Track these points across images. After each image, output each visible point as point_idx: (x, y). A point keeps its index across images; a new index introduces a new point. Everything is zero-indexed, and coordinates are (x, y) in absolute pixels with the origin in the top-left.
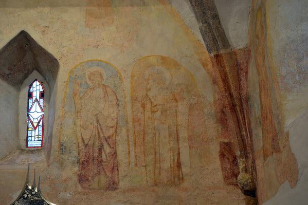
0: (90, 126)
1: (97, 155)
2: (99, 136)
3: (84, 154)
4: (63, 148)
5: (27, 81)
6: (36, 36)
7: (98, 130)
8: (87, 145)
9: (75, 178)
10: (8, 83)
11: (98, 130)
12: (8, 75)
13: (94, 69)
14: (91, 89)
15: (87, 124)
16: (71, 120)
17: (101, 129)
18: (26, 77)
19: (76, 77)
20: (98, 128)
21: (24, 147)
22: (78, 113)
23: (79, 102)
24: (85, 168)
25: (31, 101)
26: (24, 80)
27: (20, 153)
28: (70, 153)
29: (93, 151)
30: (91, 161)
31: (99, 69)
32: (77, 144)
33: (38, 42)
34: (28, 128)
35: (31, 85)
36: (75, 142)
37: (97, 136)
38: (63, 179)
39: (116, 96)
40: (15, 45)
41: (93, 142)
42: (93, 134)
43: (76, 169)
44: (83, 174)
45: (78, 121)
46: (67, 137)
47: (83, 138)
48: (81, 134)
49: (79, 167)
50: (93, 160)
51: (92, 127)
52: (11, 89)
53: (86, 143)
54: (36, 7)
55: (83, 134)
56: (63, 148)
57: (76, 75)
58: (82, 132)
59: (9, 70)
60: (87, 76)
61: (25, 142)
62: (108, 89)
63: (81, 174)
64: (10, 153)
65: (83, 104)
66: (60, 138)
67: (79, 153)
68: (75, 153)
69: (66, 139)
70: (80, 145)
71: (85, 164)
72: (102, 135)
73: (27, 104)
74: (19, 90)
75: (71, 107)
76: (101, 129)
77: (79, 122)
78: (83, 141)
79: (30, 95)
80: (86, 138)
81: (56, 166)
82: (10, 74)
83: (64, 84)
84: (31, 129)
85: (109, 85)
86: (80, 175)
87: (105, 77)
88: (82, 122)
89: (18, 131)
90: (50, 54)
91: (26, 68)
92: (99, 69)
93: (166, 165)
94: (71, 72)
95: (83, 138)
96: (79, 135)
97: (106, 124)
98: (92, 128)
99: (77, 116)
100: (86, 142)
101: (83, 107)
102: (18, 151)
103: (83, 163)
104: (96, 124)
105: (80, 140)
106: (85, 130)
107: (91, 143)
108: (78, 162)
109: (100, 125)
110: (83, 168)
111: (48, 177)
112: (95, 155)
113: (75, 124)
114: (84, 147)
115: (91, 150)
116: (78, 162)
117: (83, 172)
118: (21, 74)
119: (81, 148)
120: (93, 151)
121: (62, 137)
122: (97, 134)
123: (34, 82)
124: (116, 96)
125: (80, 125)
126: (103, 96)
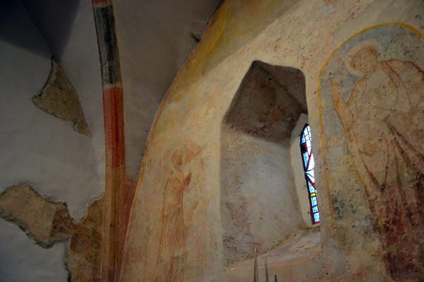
0: (379, 145)
1: (415, 201)
2: (407, 161)
3: (383, 207)
4: (337, 205)
5: (296, 131)
6: (268, 58)
7: (399, 147)
8: (384, 185)
9: (380, 267)
10: (267, 140)
11: (399, 147)
12: (262, 129)
13: (357, 48)
14: (362, 80)
15: (372, 142)
16: (340, 149)
17: (406, 142)
18: (292, 126)
19: (331, 76)
20: (397, 143)
21: (309, 224)
22: (348, 130)
23: (347, 111)
24: (395, 239)
25: (306, 155)
26: (291, 131)
27: (304, 235)
28: (354, 212)
29: (403, 196)
30: (404, 219)
31: (366, 43)
32: (363, 189)
33: (271, 64)
34: (310, 194)
35: (302, 133)
36: (357, 186)
37: (401, 160)
38: (354, 271)
39: (418, 68)
40: (253, 84)
41: (394, 176)
42: (392, 158)
43: (376, 243)
44: (395, 253)
45: (354, 144)
46: (340, 181)
47: (371, 175)
48: (365, 166)
49: (381, 239)
50: (409, 215)
51: (383, 145)
52: (275, 147)
53: (381, 182)
54: (264, 29)
55: (367, 165)
56: (337, 205)
57: (330, 73)
58: (366, 161)
59: (261, 121)
60: (348, 66)
61: (310, 215)
62: (394, 65)
63: (389, 255)
64: (287, 237)
65: (354, 113)
66: (328, 189)
67: (372, 208)
68: (364, 210)
69: (339, 187)
70: (370, 189)
71: (392, 230)
72: (411, 155)
73: (301, 160)
74: (288, 146)
75: (336, 126)
76: (406, 142)
77: (355, 148)
78: (373, 179)
79: (303, 148)
80: (378, 168)
81: (335, 247)
82: (264, 127)
83: (316, 96)
84: (314, 195)
85: (394, 56)
86: (388, 258)
87: (380, 49)
88: (360, 145)
89: (296, 202)
90: (290, 68)
91: (287, 114)
92: (366, 43)
93: (168, 269)
94: (322, 73)
95: (371, 175)
96: (362, 171)
97: (413, 127)
98: (385, 147)
99: (349, 137)
100: (381, 182)
101: (356, 116)
102: (302, 232)
103: (387, 229)
104: (391, 137)
105: (367, 180)
106: (371, 156)
107: (391, 178)
108: (376, 228)
109: (400, 135)
110: (391, 240)
111: (324, 270)
112: (409, 202)
113: (348, 152)
114: (379, 193)
115: (397, 194)
116: (376, 228)
117: (393, 249)
118: (282, 123)
119: (372, 197)
120: (403, 196)
121: (331, 185)
122: (399, 156)
123: (304, 130)
124: (418, 68)
125: (360, 151)
126: (389, 79)
